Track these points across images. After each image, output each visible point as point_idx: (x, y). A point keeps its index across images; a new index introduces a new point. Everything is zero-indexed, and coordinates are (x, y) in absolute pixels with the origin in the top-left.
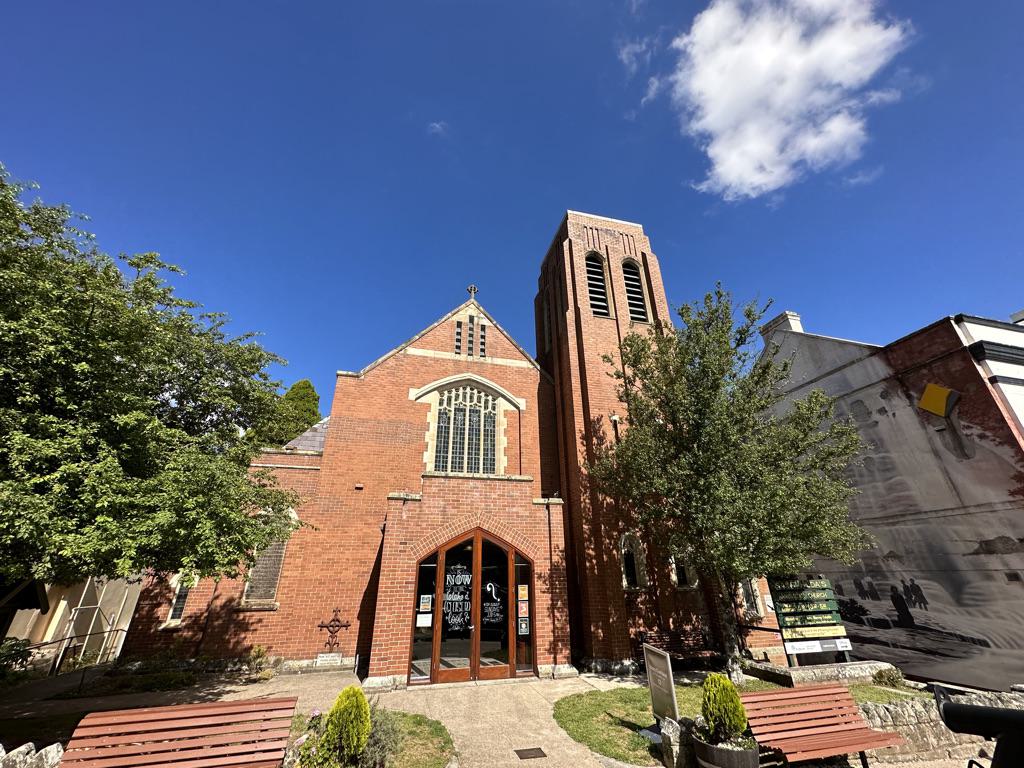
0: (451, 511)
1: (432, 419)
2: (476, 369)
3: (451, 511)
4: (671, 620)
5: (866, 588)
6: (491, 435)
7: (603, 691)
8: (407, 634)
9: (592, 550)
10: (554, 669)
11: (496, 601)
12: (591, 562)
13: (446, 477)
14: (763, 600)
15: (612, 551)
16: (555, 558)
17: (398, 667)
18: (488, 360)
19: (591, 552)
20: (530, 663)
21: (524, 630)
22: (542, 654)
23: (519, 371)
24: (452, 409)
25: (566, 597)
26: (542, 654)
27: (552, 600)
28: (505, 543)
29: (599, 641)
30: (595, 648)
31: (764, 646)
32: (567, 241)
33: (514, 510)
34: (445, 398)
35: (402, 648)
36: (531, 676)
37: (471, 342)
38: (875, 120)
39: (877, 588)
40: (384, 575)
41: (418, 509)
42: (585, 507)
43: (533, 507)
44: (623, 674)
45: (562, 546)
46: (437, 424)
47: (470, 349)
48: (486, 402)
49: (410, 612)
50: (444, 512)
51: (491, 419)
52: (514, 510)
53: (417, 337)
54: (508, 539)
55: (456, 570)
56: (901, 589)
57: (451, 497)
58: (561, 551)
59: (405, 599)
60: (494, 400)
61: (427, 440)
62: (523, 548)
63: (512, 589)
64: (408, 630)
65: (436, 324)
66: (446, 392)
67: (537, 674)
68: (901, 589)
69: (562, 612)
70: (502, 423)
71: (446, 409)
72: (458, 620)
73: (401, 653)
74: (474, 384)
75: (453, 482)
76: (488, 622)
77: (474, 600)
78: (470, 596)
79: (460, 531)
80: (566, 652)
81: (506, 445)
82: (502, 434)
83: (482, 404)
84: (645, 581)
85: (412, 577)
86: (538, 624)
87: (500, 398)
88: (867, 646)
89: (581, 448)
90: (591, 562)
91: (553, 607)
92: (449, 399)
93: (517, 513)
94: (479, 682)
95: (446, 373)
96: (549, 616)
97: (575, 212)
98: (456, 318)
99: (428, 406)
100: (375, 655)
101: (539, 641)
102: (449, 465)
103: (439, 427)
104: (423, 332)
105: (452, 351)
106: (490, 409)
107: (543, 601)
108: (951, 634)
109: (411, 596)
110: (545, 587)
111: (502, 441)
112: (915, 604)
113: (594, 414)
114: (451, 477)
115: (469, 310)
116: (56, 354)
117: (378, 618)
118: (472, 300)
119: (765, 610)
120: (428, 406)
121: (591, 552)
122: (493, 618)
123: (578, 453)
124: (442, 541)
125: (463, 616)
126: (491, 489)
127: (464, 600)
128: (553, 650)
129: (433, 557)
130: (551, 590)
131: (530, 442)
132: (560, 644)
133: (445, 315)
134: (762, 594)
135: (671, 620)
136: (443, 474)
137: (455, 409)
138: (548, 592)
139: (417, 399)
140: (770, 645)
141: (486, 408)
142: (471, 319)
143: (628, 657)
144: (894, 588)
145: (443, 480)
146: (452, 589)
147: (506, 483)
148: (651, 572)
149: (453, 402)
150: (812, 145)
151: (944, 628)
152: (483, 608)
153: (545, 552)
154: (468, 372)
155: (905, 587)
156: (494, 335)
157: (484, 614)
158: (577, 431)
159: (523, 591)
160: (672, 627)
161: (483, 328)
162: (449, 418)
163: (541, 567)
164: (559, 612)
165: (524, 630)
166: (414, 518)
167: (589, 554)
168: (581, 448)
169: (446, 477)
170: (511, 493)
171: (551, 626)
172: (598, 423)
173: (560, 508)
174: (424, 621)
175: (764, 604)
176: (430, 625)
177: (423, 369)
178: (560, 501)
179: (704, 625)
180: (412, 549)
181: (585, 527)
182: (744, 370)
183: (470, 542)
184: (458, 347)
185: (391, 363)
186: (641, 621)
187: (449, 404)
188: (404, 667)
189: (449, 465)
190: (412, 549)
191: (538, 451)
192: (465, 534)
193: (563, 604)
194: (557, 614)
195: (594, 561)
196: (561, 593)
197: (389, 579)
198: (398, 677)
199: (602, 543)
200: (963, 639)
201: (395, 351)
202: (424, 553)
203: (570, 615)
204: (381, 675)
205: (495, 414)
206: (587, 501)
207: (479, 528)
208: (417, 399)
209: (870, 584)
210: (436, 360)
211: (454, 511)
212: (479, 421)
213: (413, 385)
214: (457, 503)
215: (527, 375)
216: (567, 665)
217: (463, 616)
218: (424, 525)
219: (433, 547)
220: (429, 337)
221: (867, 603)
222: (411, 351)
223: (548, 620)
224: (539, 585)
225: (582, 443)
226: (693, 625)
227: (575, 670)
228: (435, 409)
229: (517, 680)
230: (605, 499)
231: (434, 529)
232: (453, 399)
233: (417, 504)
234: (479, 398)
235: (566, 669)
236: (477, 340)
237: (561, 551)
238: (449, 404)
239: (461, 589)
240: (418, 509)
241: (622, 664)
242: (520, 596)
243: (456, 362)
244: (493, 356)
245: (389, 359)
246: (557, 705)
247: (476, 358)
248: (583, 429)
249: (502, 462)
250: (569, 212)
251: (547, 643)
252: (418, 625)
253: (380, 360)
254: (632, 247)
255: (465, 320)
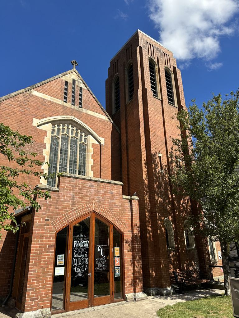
0: (77, 200)
1: (47, 140)
2: (76, 114)
3: (77, 200)
4: (185, 265)
6: (83, 157)
7: (171, 305)
8: (50, 281)
9: (150, 227)
10: (134, 295)
11: (102, 257)
12: (149, 234)
13: (75, 178)
14: (217, 254)
15: (162, 228)
16: (135, 231)
17: (44, 304)
18: (84, 110)
19: (150, 228)
20: (120, 295)
21: (117, 273)
22: (128, 287)
23: (101, 121)
24: (60, 137)
25: (140, 254)
26: (128, 287)
27: (133, 256)
28: (109, 221)
29: (153, 278)
30: (152, 282)
31: (217, 276)
32: (139, 47)
33: (113, 201)
34: (56, 129)
35: (47, 290)
36: (122, 301)
38: (223, 40)
40: (34, 241)
41: (57, 197)
42: (147, 203)
43: (123, 200)
44: (168, 295)
45: (138, 224)
46: (50, 146)
47: (73, 101)
48: (81, 136)
49: (51, 266)
50: (73, 200)
51: (84, 148)
52: (113, 201)
53: (39, 84)
54: (110, 219)
55: (80, 238)
57: (78, 191)
58: (138, 227)
59: (48, 258)
60: (85, 136)
61: (44, 155)
62: (118, 224)
63: (111, 249)
64: (50, 278)
65: (52, 79)
66: (56, 126)
67: (125, 299)
69: (139, 262)
70: (91, 151)
71: (56, 136)
72: (80, 270)
73: (45, 294)
74: (74, 124)
75: (79, 181)
76: (98, 270)
77: (90, 257)
78: (88, 254)
79: (83, 213)
80: (141, 285)
81: (92, 164)
82: (91, 158)
83: (79, 137)
84: (173, 245)
85: (53, 243)
86: (126, 270)
87: (90, 135)
89: (144, 169)
90: (149, 234)
91: (133, 260)
92: (59, 129)
93: (115, 203)
94: (95, 308)
95: (58, 113)
96: (131, 265)
97: (142, 32)
98: (64, 78)
99: (45, 133)
100: (29, 297)
101: (126, 280)
102: (68, 169)
103: (51, 147)
104: (43, 82)
105: (61, 99)
106: (83, 141)
107: (128, 256)
109: (52, 255)
110: (129, 248)
111: (90, 162)
113: (153, 151)
114: (78, 178)
115: (72, 76)
117: (31, 271)
118: (75, 70)
119: (218, 258)
120: (45, 133)
121: (150, 228)
122: (101, 267)
123: (143, 172)
124: (72, 219)
125: (84, 268)
126: (100, 187)
127: (85, 257)
128: (134, 284)
129: (65, 230)
130: (133, 250)
131: (106, 164)
132: (138, 281)
133: (58, 74)
134: (217, 251)
135: (185, 265)
136: (72, 175)
137: (62, 137)
138: (131, 251)
139: (38, 126)
140: (220, 275)
142: (74, 81)
143: (169, 286)
145: (72, 179)
146: (77, 250)
147: (109, 185)
148: (176, 240)
149: (61, 133)
150: (198, 45)
152: (95, 261)
153: (129, 227)
154: (71, 115)
156: (87, 96)
157: (96, 266)
158: (143, 160)
159: (117, 251)
160: (185, 268)
161: (81, 89)
162: (58, 143)
163: (127, 236)
164: (137, 263)
165: (117, 273)
166: (54, 203)
167: (148, 230)
168: (144, 169)
169: (75, 178)
170: (112, 191)
171: (132, 271)
172: (155, 156)
173: (137, 202)
174: (60, 272)
175: (218, 255)
176: (63, 274)
177: (43, 107)
178: (137, 198)
179: (197, 266)
180: (52, 224)
181: (147, 214)
183: (88, 220)
184: (65, 98)
185: (20, 98)
186: (172, 266)
187: (58, 133)
188: (48, 303)
189: (68, 169)
190: (52, 224)
191: (110, 170)
192: (86, 214)
193: (139, 258)
194: (136, 264)
195: (151, 234)
196: (138, 251)
197: (38, 244)
198: (44, 310)
199: (157, 223)
201: (24, 90)
202: (60, 227)
203: (143, 264)
204: (33, 310)
205: (86, 145)
206: (148, 199)
207: (94, 212)
208: (38, 126)
210: (52, 103)
211: (79, 200)
212: (77, 147)
213: (36, 117)
214: (81, 195)
215: (105, 124)
216: (141, 293)
217: (84, 268)
218: (60, 208)
219: (66, 223)
220: (47, 87)
222: (35, 93)
223: (131, 268)
224: (126, 247)
225: (145, 166)
226: (193, 267)
227: (145, 295)
228: (49, 134)
229: (115, 304)
230: (158, 199)
231: (67, 211)
232: (61, 131)
233: (56, 193)
234: (77, 133)
235: (141, 295)
236: (77, 97)
237: (138, 227)
238: (58, 133)
239: (83, 250)
240: (57, 197)
241: (167, 290)
242: (115, 254)
243: (64, 107)
244: (87, 108)
245: (19, 95)
246: (158, 312)
247: (76, 107)
248: (145, 159)
249: (90, 174)
250: (139, 30)
251: (130, 281)
252: (56, 275)
253: (13, 94)
254: (169, 62)
255: (70, 81)
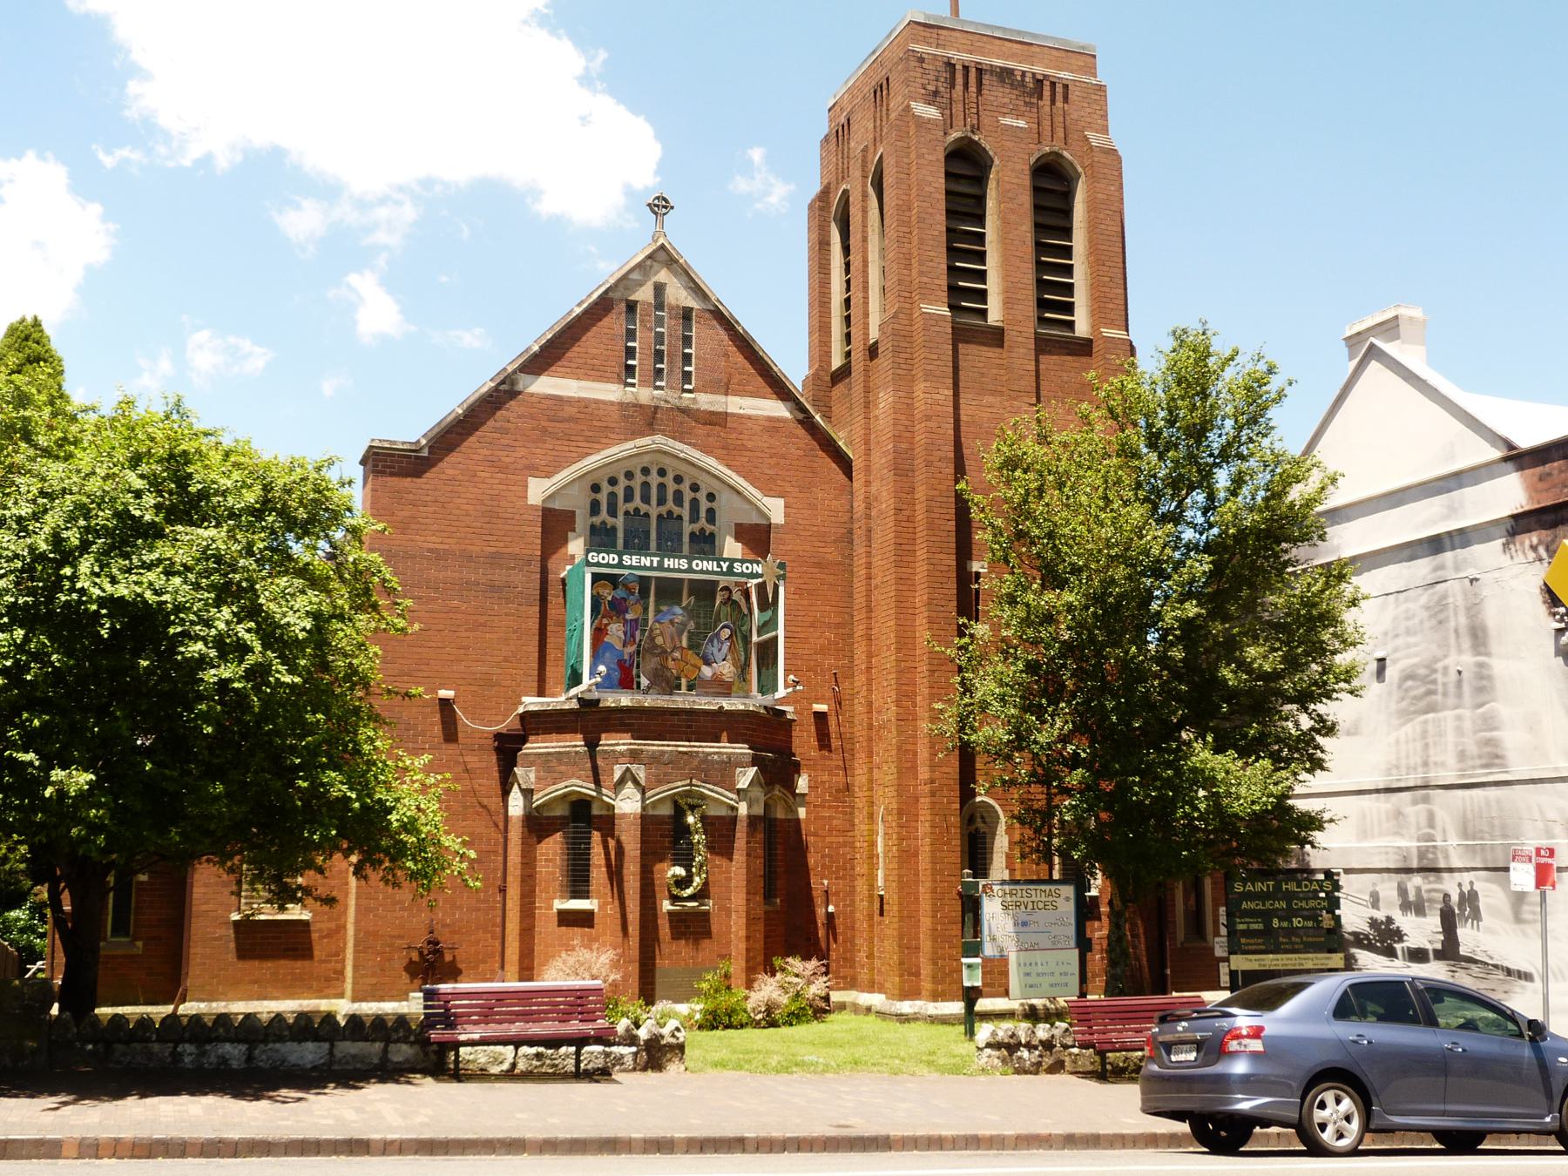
5: (1412, 897)
37: (630, 353)
39: (1425, 896)
56: (1455, 898)
68: (1455, 898)
88: (476, 1037)
108: (1496, 966)
112: (1466, 921)
116: (268, 684)
141: (694, 518)
144: (1447, 896)
151: (1491, 958)
155: (1462, 894)
182: (993, 910)
200: (1509, 972)
209: (1418, 890)
221: (1404, 922)
238: (613, 512)
